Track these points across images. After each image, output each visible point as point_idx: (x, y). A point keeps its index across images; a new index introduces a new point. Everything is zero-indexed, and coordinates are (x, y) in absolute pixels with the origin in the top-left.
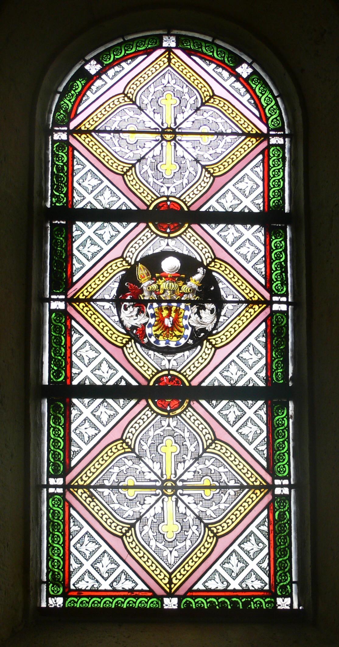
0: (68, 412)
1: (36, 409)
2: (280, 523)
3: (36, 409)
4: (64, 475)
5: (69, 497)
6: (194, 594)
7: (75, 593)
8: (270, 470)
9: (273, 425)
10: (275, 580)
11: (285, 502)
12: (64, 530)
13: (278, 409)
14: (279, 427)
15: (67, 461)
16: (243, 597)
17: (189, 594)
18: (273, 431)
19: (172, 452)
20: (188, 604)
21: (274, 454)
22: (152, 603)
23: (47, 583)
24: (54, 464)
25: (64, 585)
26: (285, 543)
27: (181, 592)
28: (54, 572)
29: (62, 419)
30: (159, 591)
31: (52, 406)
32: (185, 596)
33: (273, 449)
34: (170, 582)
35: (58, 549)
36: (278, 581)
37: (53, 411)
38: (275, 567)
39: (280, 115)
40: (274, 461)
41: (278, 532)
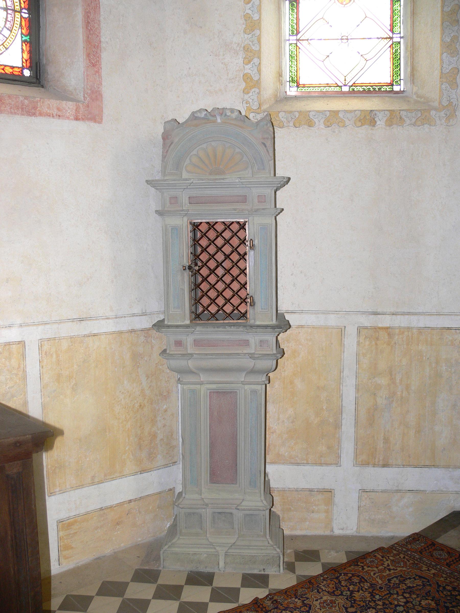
0: (298, 7)
1: (284, 4)
2: (395, 54)
3: (284, 4)
4: (297, 34)
5: (298, 44)
6: (356, 85)
7: (302, 86)
8: (392, 30)
9: (393, 10)
10: (393, 79)
11: (398, 44)
12: (297, 59)
13: (395, 2)
14: (396, 10)
15: (298, 28)
16: (378, 86)
17: (354, 85)
18: (393, 12)
19: (341, 329)
20: (353, 90)
21: (393, 23)
22: (338, 89)
23: (289, 81)
24: (292, 30)
25: (297, 82)
26: (398, 63)
27: (350, 84)
28: (292, 77)
29: (295, 4)
30: (340, 84)
31: (291, 4)
32: (352, 86)
33: (393, 21)
34: (345, 83)
35: (294, 57)
36: (394, 79)
37: (291, 6)
38: (393, 73)
39: (388, 97)
40: (393, 26)
41: (394, 58)
